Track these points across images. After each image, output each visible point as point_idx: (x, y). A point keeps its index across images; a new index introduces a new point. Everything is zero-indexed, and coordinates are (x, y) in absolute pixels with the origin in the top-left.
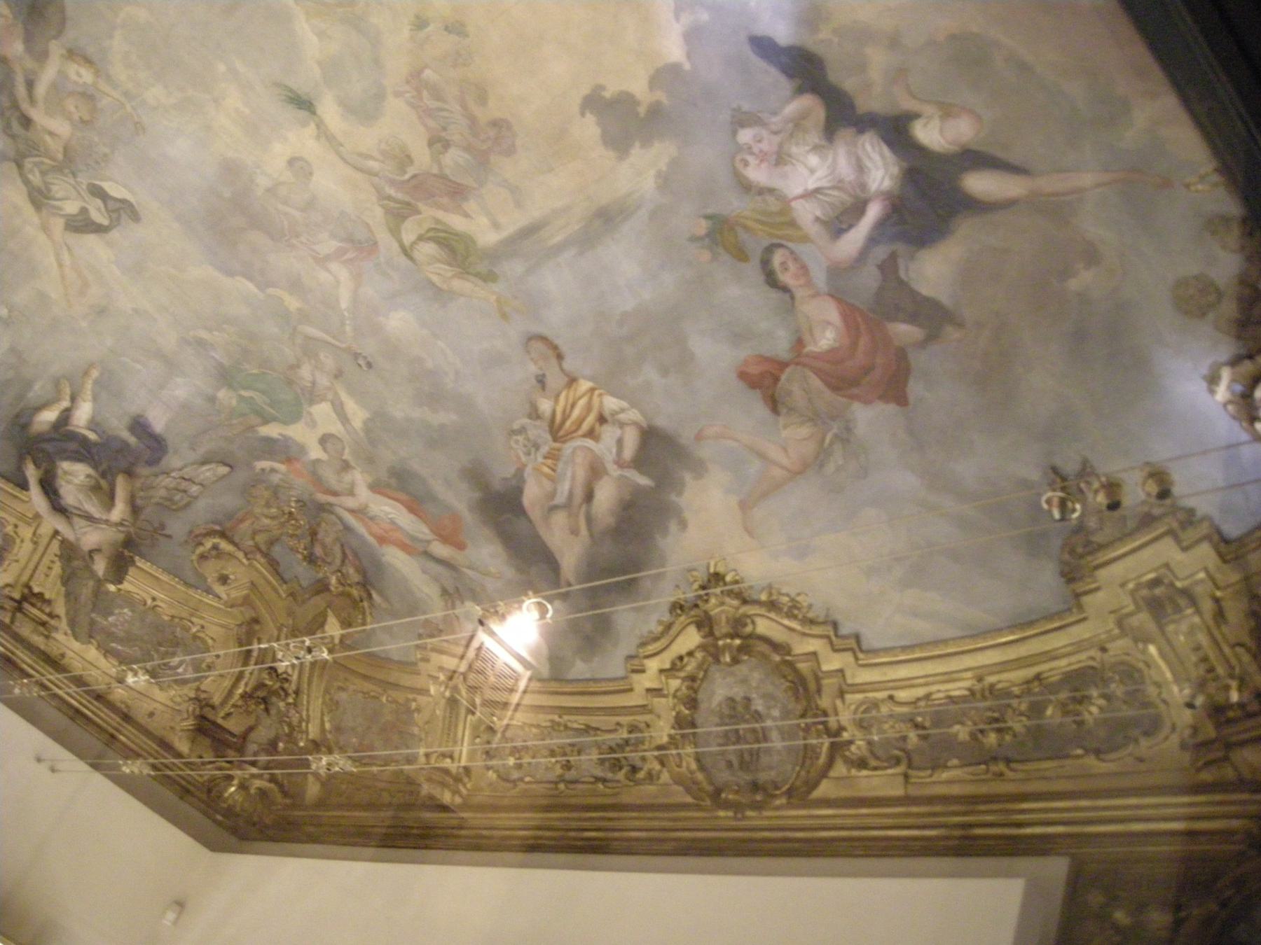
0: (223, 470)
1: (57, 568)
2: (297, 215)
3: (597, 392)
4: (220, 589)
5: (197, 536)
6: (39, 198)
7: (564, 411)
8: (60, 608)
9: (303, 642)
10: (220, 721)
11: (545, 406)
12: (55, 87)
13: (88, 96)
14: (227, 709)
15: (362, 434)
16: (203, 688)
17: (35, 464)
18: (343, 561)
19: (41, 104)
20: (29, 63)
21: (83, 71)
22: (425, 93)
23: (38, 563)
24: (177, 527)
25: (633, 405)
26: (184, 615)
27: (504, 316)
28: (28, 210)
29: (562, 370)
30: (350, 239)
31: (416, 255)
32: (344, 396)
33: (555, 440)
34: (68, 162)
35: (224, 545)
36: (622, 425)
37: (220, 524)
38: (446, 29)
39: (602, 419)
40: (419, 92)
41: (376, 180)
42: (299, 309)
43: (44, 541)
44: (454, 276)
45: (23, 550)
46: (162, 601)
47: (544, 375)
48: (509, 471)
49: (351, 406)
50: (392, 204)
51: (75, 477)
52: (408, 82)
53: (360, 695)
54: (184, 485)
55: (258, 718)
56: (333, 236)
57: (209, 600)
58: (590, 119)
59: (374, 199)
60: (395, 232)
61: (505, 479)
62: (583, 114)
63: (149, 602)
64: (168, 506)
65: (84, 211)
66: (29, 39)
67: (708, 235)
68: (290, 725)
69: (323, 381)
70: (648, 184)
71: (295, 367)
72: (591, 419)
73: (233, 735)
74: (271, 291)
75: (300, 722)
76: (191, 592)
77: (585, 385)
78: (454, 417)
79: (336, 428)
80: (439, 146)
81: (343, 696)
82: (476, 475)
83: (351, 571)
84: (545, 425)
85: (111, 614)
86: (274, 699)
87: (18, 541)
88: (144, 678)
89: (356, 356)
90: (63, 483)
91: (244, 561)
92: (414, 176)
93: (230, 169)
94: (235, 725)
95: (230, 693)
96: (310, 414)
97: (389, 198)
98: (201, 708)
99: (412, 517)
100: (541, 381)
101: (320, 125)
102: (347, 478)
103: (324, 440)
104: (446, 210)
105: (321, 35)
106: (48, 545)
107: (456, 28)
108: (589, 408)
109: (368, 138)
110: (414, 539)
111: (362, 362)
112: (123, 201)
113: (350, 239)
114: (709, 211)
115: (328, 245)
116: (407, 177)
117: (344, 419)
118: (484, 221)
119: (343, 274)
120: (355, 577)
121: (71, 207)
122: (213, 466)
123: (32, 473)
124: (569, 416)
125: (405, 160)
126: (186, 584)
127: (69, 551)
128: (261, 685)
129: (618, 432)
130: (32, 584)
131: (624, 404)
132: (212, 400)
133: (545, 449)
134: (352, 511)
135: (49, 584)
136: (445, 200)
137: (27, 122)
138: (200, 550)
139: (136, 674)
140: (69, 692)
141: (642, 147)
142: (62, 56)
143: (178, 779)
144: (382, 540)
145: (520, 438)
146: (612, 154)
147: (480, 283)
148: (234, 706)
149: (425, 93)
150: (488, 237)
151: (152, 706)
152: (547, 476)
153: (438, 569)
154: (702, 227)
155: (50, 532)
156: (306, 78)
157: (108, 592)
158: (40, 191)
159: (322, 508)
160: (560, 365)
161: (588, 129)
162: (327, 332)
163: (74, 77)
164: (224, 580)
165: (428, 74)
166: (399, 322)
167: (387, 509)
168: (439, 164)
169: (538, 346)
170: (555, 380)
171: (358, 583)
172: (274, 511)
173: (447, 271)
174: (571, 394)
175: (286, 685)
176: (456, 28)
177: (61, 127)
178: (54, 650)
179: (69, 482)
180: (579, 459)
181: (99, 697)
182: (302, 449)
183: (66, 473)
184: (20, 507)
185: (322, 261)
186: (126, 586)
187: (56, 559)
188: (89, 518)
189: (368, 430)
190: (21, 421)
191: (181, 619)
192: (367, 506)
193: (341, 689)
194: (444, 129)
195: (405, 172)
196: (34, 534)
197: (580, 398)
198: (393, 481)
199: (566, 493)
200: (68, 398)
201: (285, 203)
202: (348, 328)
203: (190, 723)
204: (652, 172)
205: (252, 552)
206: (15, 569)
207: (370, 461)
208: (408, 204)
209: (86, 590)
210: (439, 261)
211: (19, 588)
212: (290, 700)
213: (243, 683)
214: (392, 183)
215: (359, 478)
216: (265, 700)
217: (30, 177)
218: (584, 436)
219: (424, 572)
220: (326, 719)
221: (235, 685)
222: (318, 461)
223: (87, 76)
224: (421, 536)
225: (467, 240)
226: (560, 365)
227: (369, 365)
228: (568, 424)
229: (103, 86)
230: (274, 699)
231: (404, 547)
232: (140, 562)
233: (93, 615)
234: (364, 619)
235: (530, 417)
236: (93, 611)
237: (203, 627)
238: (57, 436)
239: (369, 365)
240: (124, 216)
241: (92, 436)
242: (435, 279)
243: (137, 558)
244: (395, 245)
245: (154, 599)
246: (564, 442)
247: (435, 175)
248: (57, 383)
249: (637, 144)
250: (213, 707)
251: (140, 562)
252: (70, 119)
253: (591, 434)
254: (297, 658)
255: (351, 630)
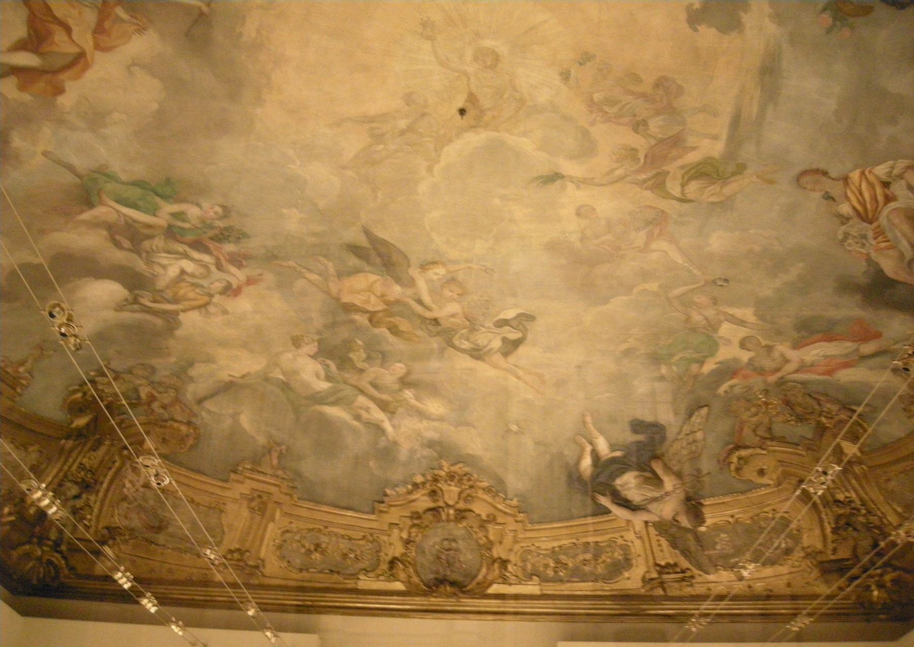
0: (704, 411)
1: (664, 543)
2: (608, 237)
3: (867, 173)
4: (765, 480)
5: (724, 461)
6: (477, 353)
7: (859, 202)
8: (684, 563)
9: (817, 471)
10: (832, 557)
11: (845, 209)
12: (432, 292)
13: (452, 280)
14: (831, 546)
15: (760, 322)
16: (805, 545)
17: (603, 495)
18: (819, 404)
19: (433, 306)
20: (410, 292)
21: (437, 270)
22: (606, 109)
23: (651, 547)
24: (706, 465)
25: (895, 159)
26: (757, 511)
27: (771, 182)
28: (479, 365)
29: (833, 179)
30: (648, 223)
31: (690, 196)
32: (731, 311)
33: (871, 223)
34: (473, 325)
35: (743, 453)
36: (901, 176)
37: (730, 443)
38: (581, 64)
39: (886, 185)
40: (601, 110)
41: (628, 179)
42: (659, 286)
43: (644, 532)
44: (721, 188)
45: (637, 547)
46: (738, 513)
47: (827, 192)
48: (862, 266)
49: (737, 312)
50: (650, 183)
51: (629, 483)
52: (591, 112)
53: (902, 475)
54: (691, 438)
55: (854, 539)
56: (637, 230)
57: (763, 491)
58: (703, 29)
59: (639, 189)
60: (668, 196)
61: (865, 272)
62: (696, 30)
63: (731, 520)
64: (695, 457)
65: (504, 340)
66: (398, 280)
67: (835, 19)
68: (876, 527)
69: (710, 313)
70: (772, 28)
71: (688, 319)
72: (879, 190)
73: (848, 560)
74: (635, 291)
75: (881, 521)
76: (749, 495)
77: (855, 175)
78: (801, 265)
79: (743, 332)
80: (641, 128)
81: (892, 484)
82: (846, 286)
83: (829, 406)
84: (856, 220)
85: (716, 543)
86: (853, 519)
87: (630, 544)
88: (751, 567)
89: (714, 282)
90: (626, 492)
91: (764, 452)
92: (646, 156)
93: (553, 247)
94: (844, 553)
95: (824, 536)
96: (721, 337)
97: (645, 181)
98: (814, 558)
99: (834, 343)
100: (828, 197)
101: (572, 179)
102: (776, 354)
103: (743, 345)
104: (680, 157)
105: (525, 134)
106: (648, 534)
107: (585, 58)
108: (871, 185)
109: (602, 162)
110: (847, 355)
111: (720, 283)
112: (519, 315)
113: (648, 223)
114: (820, 7)
115: (640, 238)
116: (642, 160)
117: (742, 323)
118: (706, 141)
119: (663, 245)
120: (835, 408)
121: (497, 344)
122: (696, 413)
123: (605, 501)
124: (864, 201)
125: (632, 153)
126: (742, 493)
127: (665, 528)
128: (838, 517)
129: (903, 182)
130: (658, 562)
131: (890, 163)
132: (662, 378)
133: (870, 234)
134: (797, 371)
135: (667, 555)
136: (674, 153)
137: (436, 322)
138: (733, 467)
139: (744, 568)
140: (722, 607)
141: (746, 12)
142: (420, 272)
143: (829, 611)
144: (830, 373)
145: (850, 241)
146: (734, 34)
147: (738, 177)
148: (833, 542)
149: (606, 109)
150: (717, 149)
151: (785, 579)
152: (887, 248)
153: (878, 360)
154: (827, 18)
155: (643, 525)
156: (542, 162)
157: (703, 533)
158: (474, 350)
159: (781, 382)
160: (830, 178)
161: (707, 35)
162: (685, 284)
163: (435, 277)
164: (761, 472)
165: (597, 97)
166: (718, 241)
167: (815, 352)
168: (651, 136)
169: (806, 179)
170: (836, 189)
171: (839, 410)
172: (753, 410)
173: (716, 188)
174: (853, 187)
175: (853, 505)
176: (585, 58)
177: (453, 308)
178: (699, 590)
179: (629, 489)
180: (897, 221)
181: (768, 597)
182: (736, 360)
183: (621, 486)
184: (614, 524)
185: (645, 249)
186: (709, 522)
187: (660, 538)
188: (655, 500)
189: (761, 318)
190: (574, 478)
191: (758, 515)
192: (803, 360)
193: (888, 480)
194: (635, 115)
195: (639, 159)
196: (635, 533)
197: (860, 186)
198: (804, 333)
199: (909, 248)
200: (587, 444)
201: (597, 237)
202: (695, 271)
203: (816, 573)
204: (767, 20)
205: (764, 443)
206: (641, 560)
207: (779, 332)
208: (658, 174)
209: (692, 543)
210: (705, 187)
211: (652, 569)
212: (864, 512)
213: (826, 524)
214: (638, 172)
215: (783, 348)
216: (848, 524)
217: (464, 347)
218: (885, 204)
219: (871, 369)
220: (895, 506)
221: (823, 529)
222: (750, 360)
223: (441, 271)
224: (849, 350)
225: (708, 161)
226: (830, 178)
227: (726, 280)
228: (869, 206)
229: (452, 268)
230: (853, 519)
231: (847, 365)
232: (707, 502)
233: (707, 553)
234: (862, 427)
235: (843, 224)
236: (703, 550)
237: (774, 510)
238: (600, 470)
239: (726, 280)
240: (525, 323)
241: (618, 454)
242: (714, 199)
243: (702, 501)
244: (674, 202)
245: (732, 516)
246: (877, 219)
247: (656, 145)
248: (575, 442)
249: (742, 14)
250: (821, 552)
251: (707, 502)
252: (454, 300)
253: (888, 199)
254: (823, 483)
255: (862, 441)
